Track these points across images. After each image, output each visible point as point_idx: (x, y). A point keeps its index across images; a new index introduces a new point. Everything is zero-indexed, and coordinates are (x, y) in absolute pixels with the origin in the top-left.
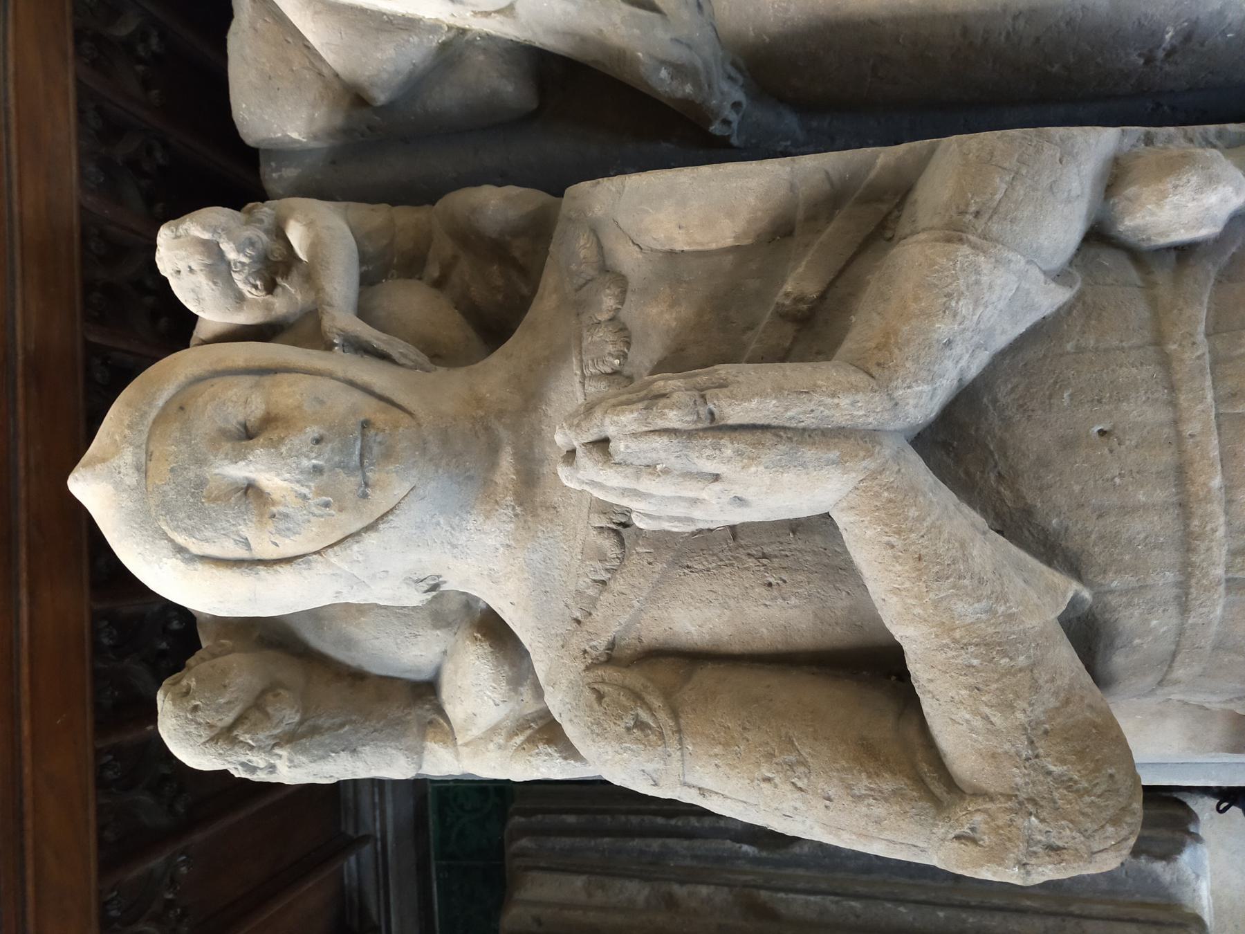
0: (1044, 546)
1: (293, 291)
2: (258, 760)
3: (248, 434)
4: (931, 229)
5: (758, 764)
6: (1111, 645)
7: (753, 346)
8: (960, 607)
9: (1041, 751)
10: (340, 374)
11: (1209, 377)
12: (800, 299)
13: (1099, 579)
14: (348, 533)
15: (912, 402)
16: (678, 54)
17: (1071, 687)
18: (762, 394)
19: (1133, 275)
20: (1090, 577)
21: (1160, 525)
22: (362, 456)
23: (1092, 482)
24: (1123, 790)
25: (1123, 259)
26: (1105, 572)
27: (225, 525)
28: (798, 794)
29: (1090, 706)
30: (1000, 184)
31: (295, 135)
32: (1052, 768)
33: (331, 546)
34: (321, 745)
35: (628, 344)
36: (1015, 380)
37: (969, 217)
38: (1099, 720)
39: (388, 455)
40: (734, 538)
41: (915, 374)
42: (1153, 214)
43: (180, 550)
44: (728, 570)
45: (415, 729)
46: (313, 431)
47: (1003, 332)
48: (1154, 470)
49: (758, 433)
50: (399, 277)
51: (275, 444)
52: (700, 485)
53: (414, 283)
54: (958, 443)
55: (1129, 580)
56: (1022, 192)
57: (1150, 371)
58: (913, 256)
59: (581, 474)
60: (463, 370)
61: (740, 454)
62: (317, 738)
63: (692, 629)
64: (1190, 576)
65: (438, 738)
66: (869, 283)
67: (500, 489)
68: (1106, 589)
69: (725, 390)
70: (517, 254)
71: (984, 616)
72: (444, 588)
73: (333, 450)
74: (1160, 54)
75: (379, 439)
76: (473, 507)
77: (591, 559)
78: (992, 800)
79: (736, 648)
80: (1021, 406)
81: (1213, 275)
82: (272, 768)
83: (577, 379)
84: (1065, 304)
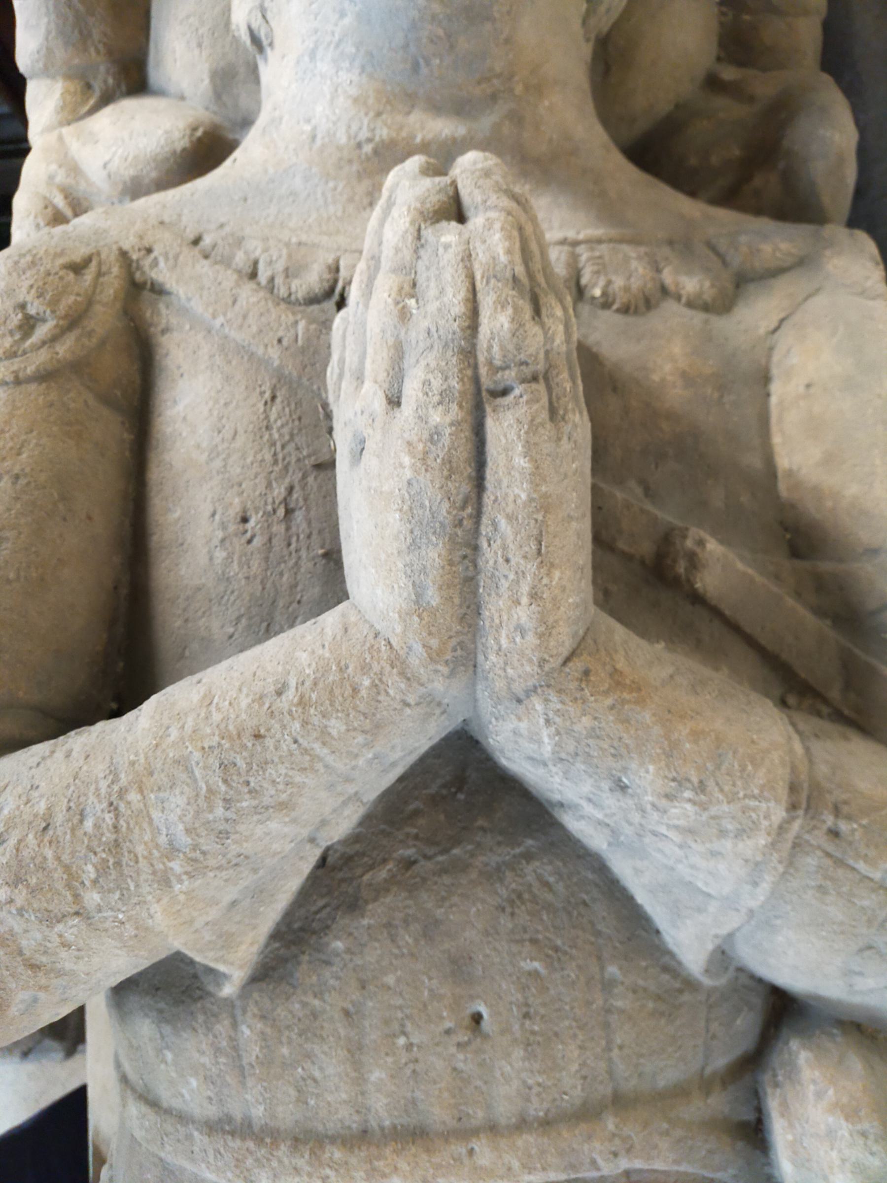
0: (302, 929)
4: (811, 761)
6: (162, 1018)
7: (619, 495)
8: (178, 800)
13: (253, 1009)
15: (523, 726)
17: (60, 973)
18: (537, 475)
19: (721, 1061)
20: (256, 995)
21: (335, 1105)
23: (399, 1002)
25: (746, 1044)
26: (263, 1017)
35: (625, 310)
36: (560, 887)
40: (319, 467)
41: (570, 732)
42: (819, 1095)
44: (268, 457)
45: (76, 61)
47: (637, 871)
48: (418, 1094)
49: (469, 471)
50: (722, 24)
52: (382, 376)
54: (461, 802)
55: (253, 1052)
56: (866, 903)
57: (573, 1091)
58: (769, 734)
61: (434, 437)
63: (180, 407)
64: (259, 1140)
65: (68, 98)
66: (717, 669)
67: (399, 118)
68: (239, 1018)
69: (545, 415)
70: (758, 181)
71: (162, 840)
76: (371, 76)
77: (290, 256)
79: (154, 474)
80: (520, 896)
83: (571, 234)
84: (679, 963)
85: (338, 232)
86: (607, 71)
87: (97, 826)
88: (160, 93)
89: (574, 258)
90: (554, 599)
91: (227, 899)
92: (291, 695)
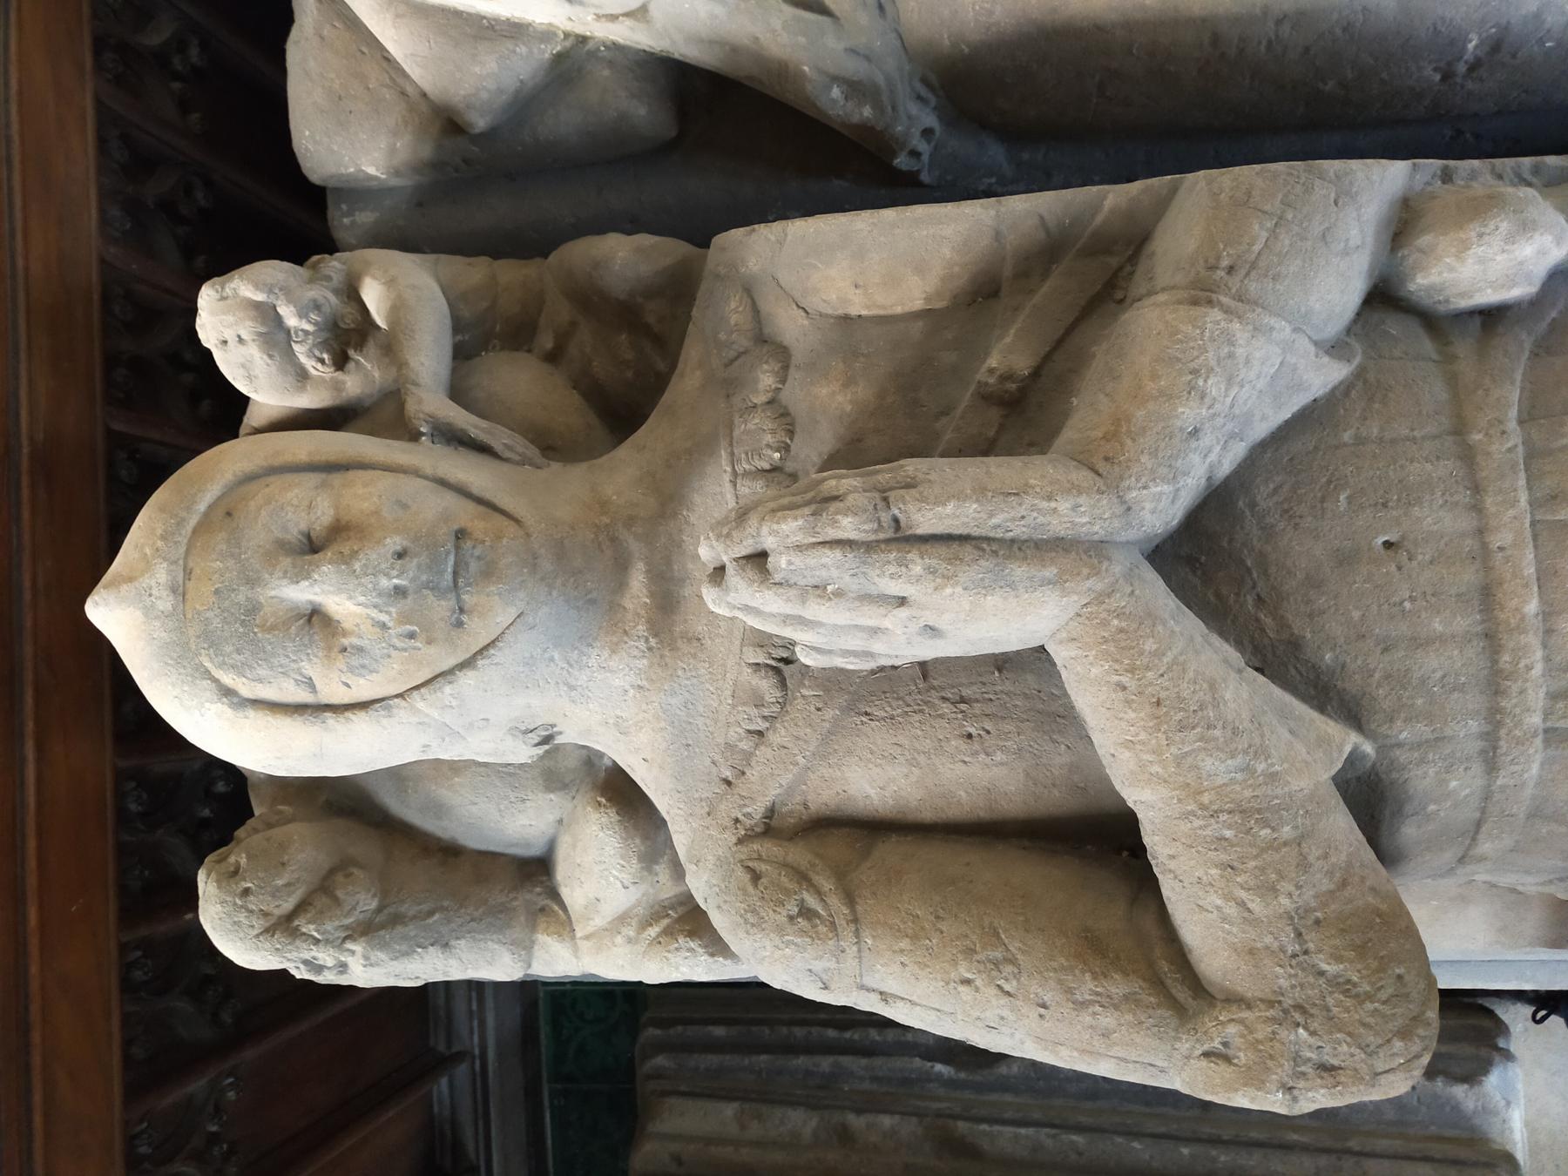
0: (1316, 687)
1: (369, 366)
2: (325, 957)
3: (312, 546)
4: (1173, 288)
5: (954, 963)
6: (1399, 813)
7: (948, 436)
8: (1208, 764)
9: (1311, 946)
10: (429, 471)
11: (1522, 475)
12: (1007, 377)
13: (1384, 729)
14: (438, 671)
15: (1148, 506)
16: (854, 68)
17: (1349, 864)
18: (960, 497)
19: (1427, 346)
20: (1373, 727)
21: (1461, 661)
22: (455, 574)
23: (1375, 607)
24: (1414, 995)
25: (1414, 326)
26: (1391, 720)
27: (284, 661)
28: (1005, 1000)
29: (1373, 889)
30: (1259, 231)
31: (371, 171)
32: (1325, 967)
33: (417, 688)
34: (405, 938)
35: (791, 433)
36: (1278, 479)
37: (1221, 273)
38: (1384, 907)
39: (489, 572)
40: (925, 676)
42: (1451, 269)
43: (227, 693)
44: (917, 717)
45: (522, 919)
46: (394, 542)
47: (1264, 418)
49: (955, 546)
50: (502, 349)
51: (346, 559)
52: (882, 610)
53: (521, 356)
54: (1207, 558)
55: (1422, 730)
56: (1287, 242)
57: (1448, 467)
58: (1150, 322)
59: (732, 597)
60: (584, 466)
61: (932, 571)
62: (400, 929)
63: (872, 792)
64: (1498, 725)
65: (552, 929)
66: (1094, 356)
67: (629, 616)
68: (1393, 741)
69: (913, 491)
70: (651, 319)
71: (1239, 776)
72: (559, 740)
73: (419, 566)
74: (1462, 68)
75: (477, 552)
76: (595, 639)
77: (744, 704)
78: (1249, 1007)
79: (927, 816)
80: (1286, 511)
81: (1528, 346)
82: (343, 967)
83: (727, 477)
84: (1341, 383)
85: (724, 665)
87: (1229, 827)
90: (1051, 483)
91: (1288, 735)
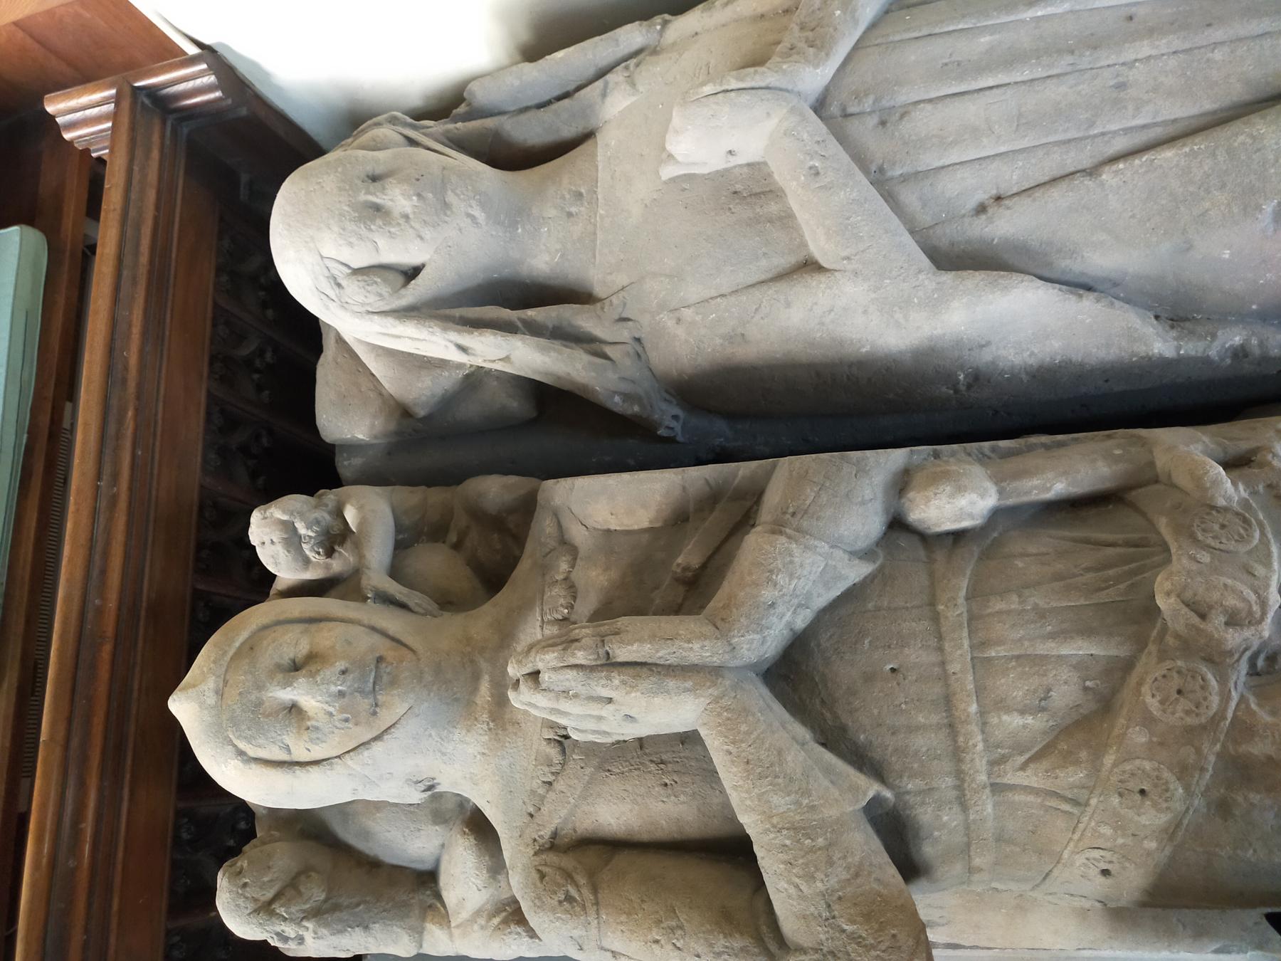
2: (290, 930)
3: (295, 667)
5: (650, 929)
7: (657, 602)
9: (836, 913)
10: (366, 622)
11: (966, 630)
12: (685, 569)
16: (624, 387)
19: (922, 553)
22: (374, 683)
25: (915, 539)
27: (274, 735)
28: (677, 953)
29: (877, 880)
30: (810, 493)
31: (361, 436)
32: (846, 927)
33: (348, 752)
34: (340, 920)
35: (575, 598)
37: (788, 516)
38: (885, 892)
39: (394, 683)
40: (641, 748)
43: (241, 753)
44: (636, 773)
46: (341, 665)
47: (819, 595)
49: (638, 668)
51: (312, 675)
54: (794, 676)
57: (925, 624)
58: (753, 541)
60: (463, 615)
61: (624, 683)
62: (337, 914)
63: (612, 821)
64: (963, 781)
71: (792, 807)
74: (963, 388)
78: (805, 953)
79: (645, 837)
81: (976, 555)
82: (301, 940)
83: (538, 624)
86: (450, 603)
88: (438, 862)
89: (549, 622)
92: (730, 748)
